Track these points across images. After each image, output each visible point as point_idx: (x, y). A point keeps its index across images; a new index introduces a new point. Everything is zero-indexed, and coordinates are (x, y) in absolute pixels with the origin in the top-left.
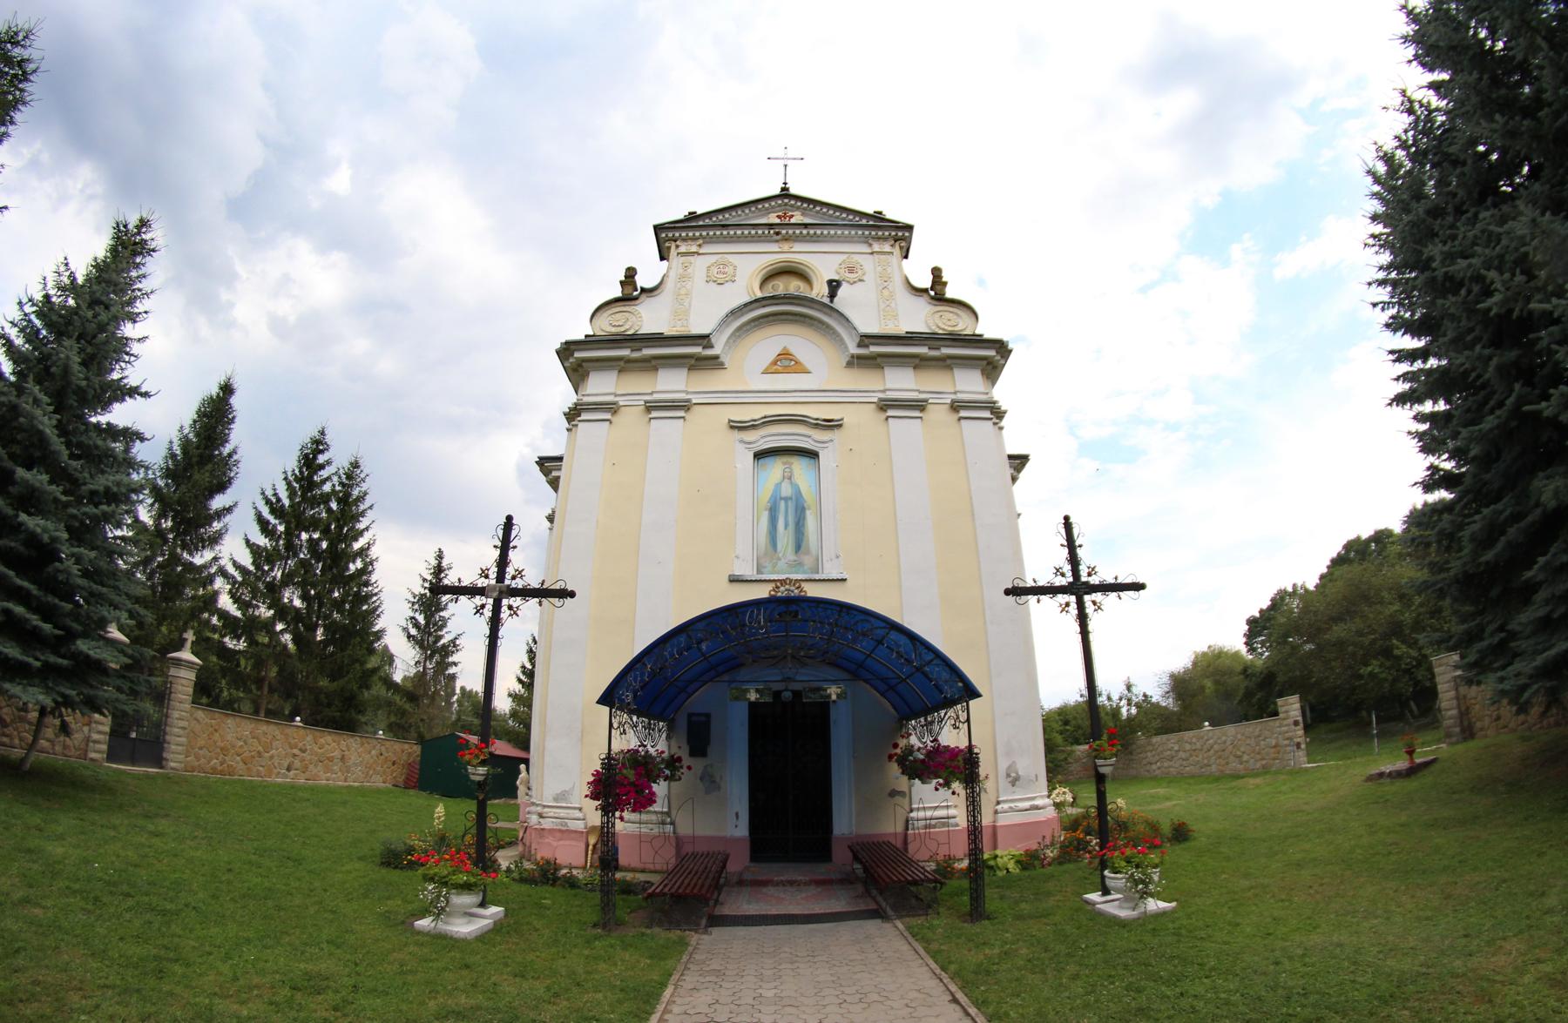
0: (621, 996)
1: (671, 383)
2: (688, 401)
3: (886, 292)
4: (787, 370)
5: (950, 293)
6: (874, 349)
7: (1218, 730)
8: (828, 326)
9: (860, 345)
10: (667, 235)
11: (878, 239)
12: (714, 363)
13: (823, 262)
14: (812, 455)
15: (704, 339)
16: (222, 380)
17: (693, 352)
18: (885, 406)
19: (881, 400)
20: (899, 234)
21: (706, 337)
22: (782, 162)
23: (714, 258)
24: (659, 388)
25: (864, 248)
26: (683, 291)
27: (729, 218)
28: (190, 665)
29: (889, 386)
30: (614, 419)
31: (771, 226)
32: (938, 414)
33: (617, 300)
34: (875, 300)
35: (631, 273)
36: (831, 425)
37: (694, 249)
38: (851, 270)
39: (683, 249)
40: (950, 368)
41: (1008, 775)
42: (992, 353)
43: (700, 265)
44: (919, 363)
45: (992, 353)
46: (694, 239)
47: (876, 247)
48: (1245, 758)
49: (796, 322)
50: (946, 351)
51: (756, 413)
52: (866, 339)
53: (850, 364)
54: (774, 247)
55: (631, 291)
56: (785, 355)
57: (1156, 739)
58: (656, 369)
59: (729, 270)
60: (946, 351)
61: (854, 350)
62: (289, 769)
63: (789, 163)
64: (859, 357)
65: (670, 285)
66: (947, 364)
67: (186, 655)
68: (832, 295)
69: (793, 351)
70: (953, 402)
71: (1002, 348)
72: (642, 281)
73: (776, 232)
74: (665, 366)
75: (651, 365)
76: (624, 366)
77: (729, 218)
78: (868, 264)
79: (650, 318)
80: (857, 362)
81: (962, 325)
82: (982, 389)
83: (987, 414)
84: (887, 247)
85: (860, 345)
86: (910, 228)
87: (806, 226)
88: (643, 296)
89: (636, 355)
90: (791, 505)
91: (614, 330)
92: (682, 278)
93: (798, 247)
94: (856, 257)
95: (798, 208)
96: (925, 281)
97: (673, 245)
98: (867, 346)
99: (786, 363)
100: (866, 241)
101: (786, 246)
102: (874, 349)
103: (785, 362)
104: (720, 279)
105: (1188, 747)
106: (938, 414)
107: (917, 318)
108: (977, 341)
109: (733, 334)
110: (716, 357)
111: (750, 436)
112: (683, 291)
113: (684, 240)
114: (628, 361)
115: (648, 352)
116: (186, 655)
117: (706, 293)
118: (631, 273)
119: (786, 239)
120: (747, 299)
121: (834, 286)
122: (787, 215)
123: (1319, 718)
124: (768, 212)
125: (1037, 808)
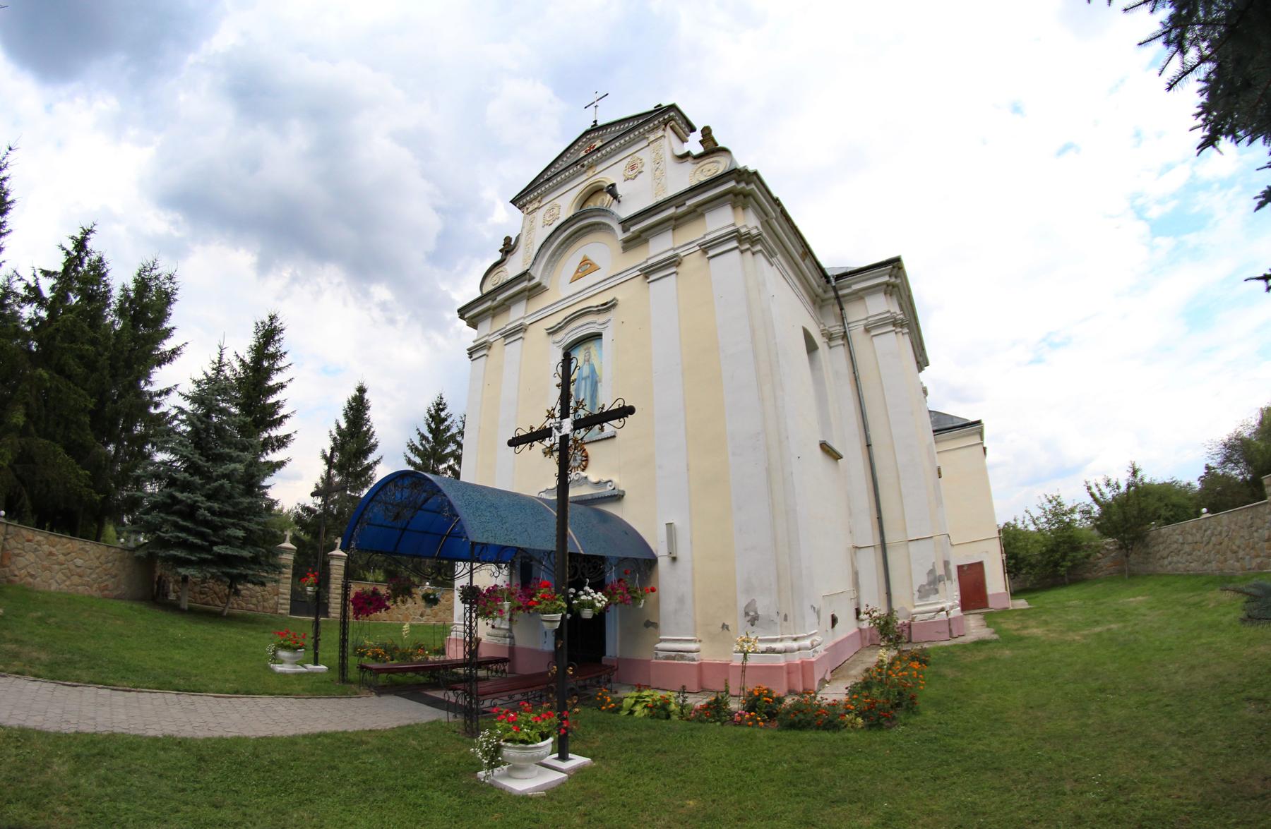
0: (386, 795)
1: (517, 314)
2: (677, 255)
7: (1224, 516)
12: (537, 290)
14: (597, 336)
16: (357, 385)
18: (648, 272)
24: (709, 230)
27: (559, 167)
28: (339, 557)
30: (679, 270)
32: (693, 262)
36: (608, 307)
41: (747, 614)
45: (732, 184)
46: (535, 198)
48: (1241, 554)
49: (590, 232)
51: (559, 318)
54: (584, 177)
56: (585, 261)
57: (1165, 530)
58: (702, 215)
62: (422, 615)
67: (338, 552)
77: (559, 167)
80: (630, 244)
83: (734, 244)
84: (660, 133)
90: (589, 382)
101: (590, 173)
103: (587, 266)
105: (1190, 538)
106: (693, 262)
110: (539, 284)
111: (558, 337)
114: (495, 308)
115: (500, 298)
116: (338, 552)
119: (591, 167)
123: (1212, 510)
125: (773, 651)
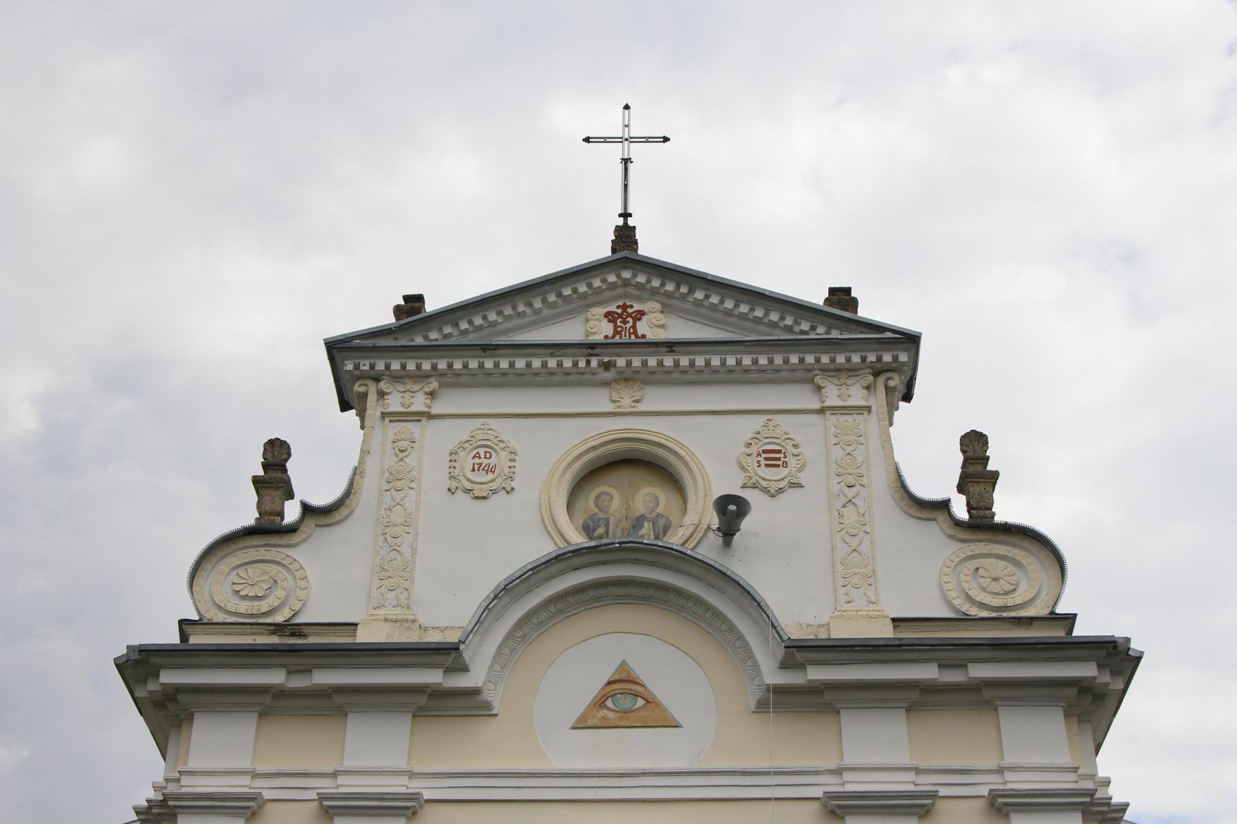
2: (415, 797)
3: (850, 515)
4: (628, 720)
5: (1005, 509)
6: (817, 674)
8: (717, 614)
9: (785, 665)
10: (356, 364)
11: (836, 371)
12: (467, 705)
13: (711, 437)
15: (446, 654)
17: (426, 683)
19: (830, 796)
20: (889, 359)
21: (450, 649)
22: (616, 151)
23: (463, 430)
25: (801, 397)
26: (397, 516)
29: (850, 760)
31: (591, 348)
33: (248, 532)
34: (819, 569)
35: (276, 455)
37: (419, 403)
38: (773, 458)
39: (394, 403)
40: (990, 706)
42: (1087, 670)
43: (435, 444)
44: (920, 699)
45: (1087, 670)
46: (420, 376)
47: (833, 395)
49: (646, 600)
50: (979, 671)
52: (799, 652)
53: (762, 706)
54: (598, 400)
55: (275, 517)
58: (341, 713)
59: (500, 460)
60: (979, 671)
61: (773, 676)
63: (636, 151)
64: (779, 690)
65: (367, 496)
66: (982, 698)
68: (728, 530)
69: (641, 671)
70: (994, 796)
71: (1118, 658)
72: (313, 482)
73: (603, 363)
74: (364, 709)
75: (332, 705)
76: (271, 705)
78: (810, 439)
79: (328, 586)
80: (780, 701)
81: (1023, 588)
82: (1065, 760)
84: (857, 396)
85: (785, 665)
86: (911, 341)
87: (671, 346)
88: (310, 524)
89: (298, 683)
91: (244, 607)
92: (396, 480)
93: (655, 399)
94: (783, 421)
95: (654, 293)
96: (937, 476)
97: (372, 389)
98: (801, 667)
99: (626, 702)
100: (806, 377)
102: (817, 674)
103: (624, 702)
104: (481, 478)
107: (919, 582)
108: (1057, 639)
109: (510, 635)
110: (475, 692)
112: (397, 516)
113: (397, 378)
117: (451, 533)
118: (276, 455)
119: (629, 378)
120: (544, 548)
121: (731, 511)
122: (632, 314)
124: (584, 304)
